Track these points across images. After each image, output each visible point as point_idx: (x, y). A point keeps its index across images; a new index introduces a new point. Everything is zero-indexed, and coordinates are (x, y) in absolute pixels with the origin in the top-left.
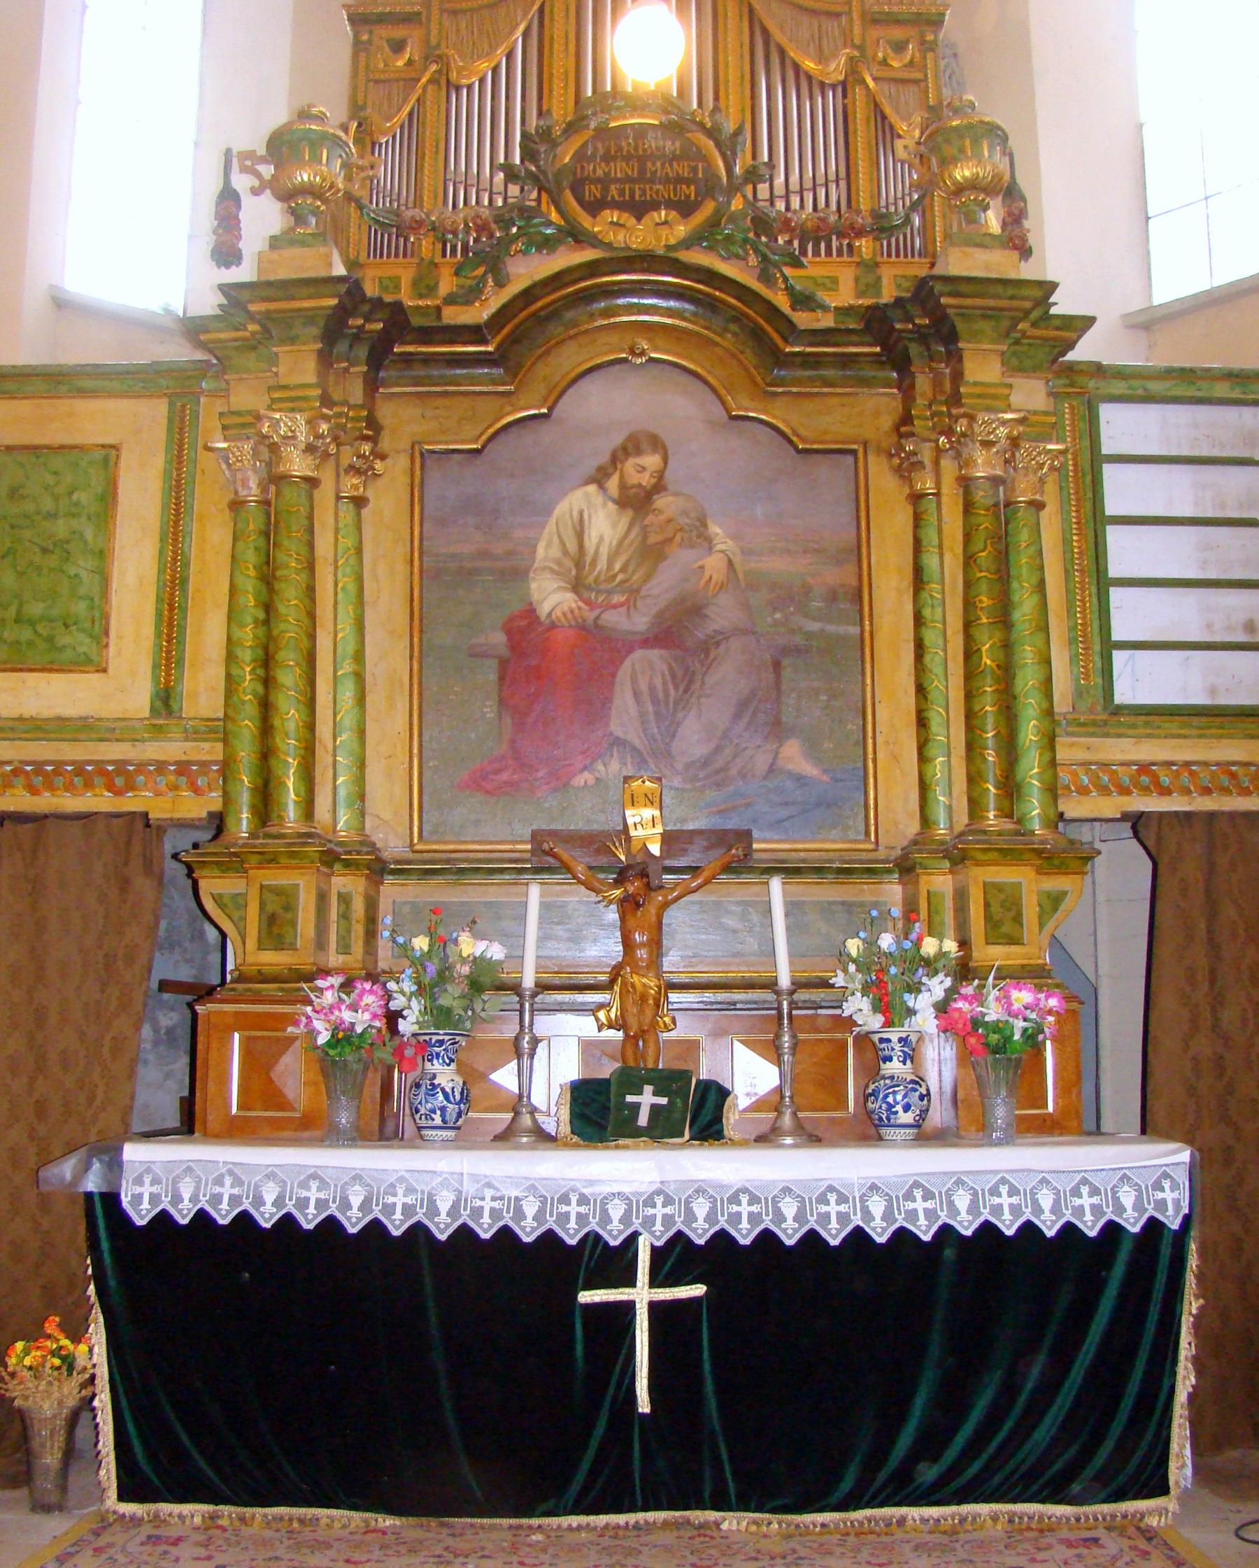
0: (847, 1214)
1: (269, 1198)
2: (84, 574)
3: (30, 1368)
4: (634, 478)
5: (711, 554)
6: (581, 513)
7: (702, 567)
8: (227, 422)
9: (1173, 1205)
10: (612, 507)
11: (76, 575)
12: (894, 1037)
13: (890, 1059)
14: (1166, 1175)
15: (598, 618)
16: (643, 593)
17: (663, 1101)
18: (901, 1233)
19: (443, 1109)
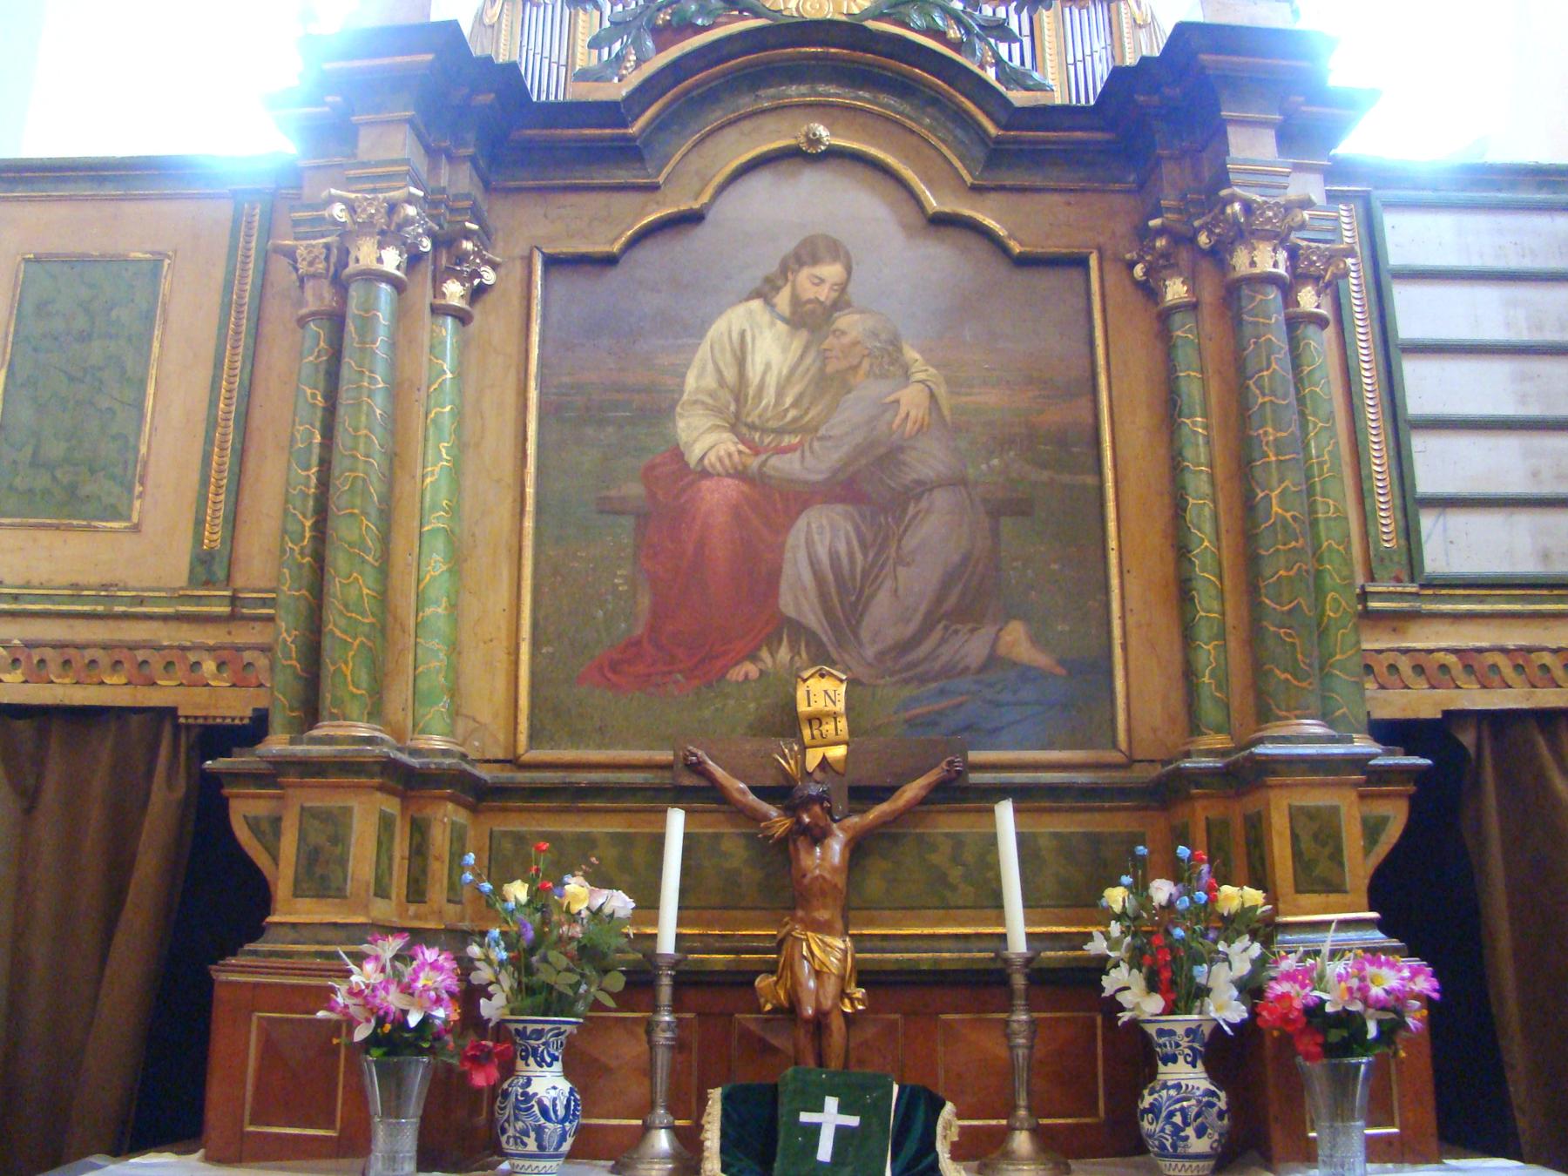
2: (117, 406)
4: (809, 292)
6: (742, 334)
7: (897, 402)
10: (781, 327)
12: (1180, 1030)
13: (1174, 1059)
15: (764, 463)
17: (853, 1121)
19: (539, 1130)
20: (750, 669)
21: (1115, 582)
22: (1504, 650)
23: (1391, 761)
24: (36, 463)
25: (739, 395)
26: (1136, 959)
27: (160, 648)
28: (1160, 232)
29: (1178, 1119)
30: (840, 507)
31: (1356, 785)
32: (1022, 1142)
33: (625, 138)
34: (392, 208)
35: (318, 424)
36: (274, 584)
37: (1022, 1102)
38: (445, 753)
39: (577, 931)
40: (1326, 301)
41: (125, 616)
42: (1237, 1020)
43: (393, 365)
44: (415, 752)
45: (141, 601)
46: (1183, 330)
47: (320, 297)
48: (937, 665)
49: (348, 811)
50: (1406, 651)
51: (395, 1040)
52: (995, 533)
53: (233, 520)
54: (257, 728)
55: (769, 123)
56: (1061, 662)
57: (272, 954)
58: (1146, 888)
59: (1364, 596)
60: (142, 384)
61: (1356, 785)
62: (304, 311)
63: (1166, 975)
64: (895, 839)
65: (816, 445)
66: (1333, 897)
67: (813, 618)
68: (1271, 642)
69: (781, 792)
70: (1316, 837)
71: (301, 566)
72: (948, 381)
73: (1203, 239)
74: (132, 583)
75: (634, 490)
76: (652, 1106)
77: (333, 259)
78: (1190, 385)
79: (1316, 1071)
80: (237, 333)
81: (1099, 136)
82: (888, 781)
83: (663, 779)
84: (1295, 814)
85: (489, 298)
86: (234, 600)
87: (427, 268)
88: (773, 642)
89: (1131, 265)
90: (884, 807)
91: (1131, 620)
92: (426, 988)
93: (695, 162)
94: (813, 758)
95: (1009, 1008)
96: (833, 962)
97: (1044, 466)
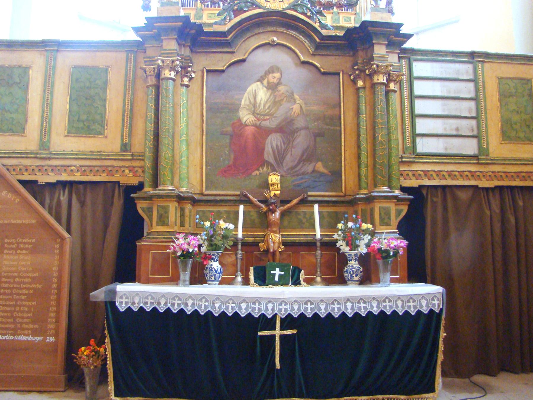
0: (340, 308)
1: (163, 303)
2: (99, 106)
3: (86, 356)
4: (272, 80)
5: (295, 104)
6: (255, 91)
7: (293, 108)
8: (146, 59)
9: (437, 305)
10: (265, 89)
11: (97, 107)
12: (353, 254)
13: (351, 260)
14: (435, 296)
15: (261, 123)
16: (275, 115)
17: (283, 273)
18: (356, 314)
19: (215, 275)
20: (257, 172)
21: (343, 153)
22: (434, 171)
23: (404, 197)
24: (79, 120)
25: (255, 106)
26: (344, 239)
27: (114, 167)
28: (357, 69)
29: (352, 273)
30: (278, 134)
31: (395, 202)
32: (318, 279)
33: (226, 40)
34: (173, 62)
35: (153, 112)
36: (143, 151)
37: (319, 270)
38: (188, 192)
39: (222, 232)
40: (398, 85)
41: (105, 159)
42: (365, 252)
43: (173, 100)
44: (182, 192)
45: (109, 155)
46: (362, 93)
47: (152, 81)
48: (301, 172)
49: (168, 206)
50: (411, 171)
51: (186, 255)
52: (315, 141)
53: (130, 135)
54: (141, 186)
55: (262, 36)
56: (330, 172)
57: (153, 238)
58: (347, 223)
59: (402, 158)
60: (105, 100)
61: (395, 202)
62: (148, 84)
63: (350, 242)
64: (290, 212)
65: (273, 119)
66: (389, 227)
67: (272, 160)
68: (377, 170)
69: (265, 201)
70: (385, 213)
71: (151, 148)
72: (305, 104)
73: (367, 72)
74: (106, 151)
75: (229, 129)
76: (237, 272)
77: (156, 72)
78: (363, 108)
79: (380, 262)
80: (129, 88)
81: (343, 42)
82: (289, 199)
83: (238, 198)
84: (380, 208)
85: (192, 80)
86: (132, 155)
87: (179, 74)
88: (262, 166)
89: (350, 75)
90: (288, 205)
91: (346, 162)
92: (193, 244)
93: (244, 46)
94: (272, 194)
95: (316, 250)
96: (277, 240)
97: (327, 125)
